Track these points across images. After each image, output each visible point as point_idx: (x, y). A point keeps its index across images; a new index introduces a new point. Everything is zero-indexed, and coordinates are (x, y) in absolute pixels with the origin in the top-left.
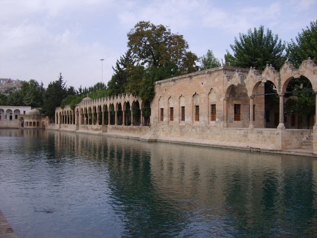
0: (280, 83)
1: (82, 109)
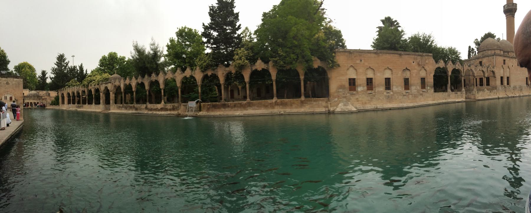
0: (463, 71)
1: (69, 94)
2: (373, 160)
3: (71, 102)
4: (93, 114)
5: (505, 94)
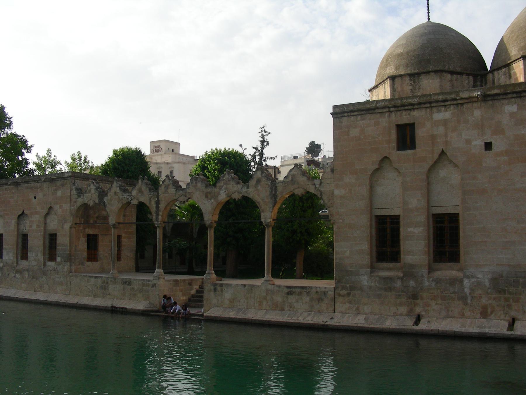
0: (157, 207)
2: (29, 392)
3: (202, 299)
4: (4, 297)
5: (403, 310)
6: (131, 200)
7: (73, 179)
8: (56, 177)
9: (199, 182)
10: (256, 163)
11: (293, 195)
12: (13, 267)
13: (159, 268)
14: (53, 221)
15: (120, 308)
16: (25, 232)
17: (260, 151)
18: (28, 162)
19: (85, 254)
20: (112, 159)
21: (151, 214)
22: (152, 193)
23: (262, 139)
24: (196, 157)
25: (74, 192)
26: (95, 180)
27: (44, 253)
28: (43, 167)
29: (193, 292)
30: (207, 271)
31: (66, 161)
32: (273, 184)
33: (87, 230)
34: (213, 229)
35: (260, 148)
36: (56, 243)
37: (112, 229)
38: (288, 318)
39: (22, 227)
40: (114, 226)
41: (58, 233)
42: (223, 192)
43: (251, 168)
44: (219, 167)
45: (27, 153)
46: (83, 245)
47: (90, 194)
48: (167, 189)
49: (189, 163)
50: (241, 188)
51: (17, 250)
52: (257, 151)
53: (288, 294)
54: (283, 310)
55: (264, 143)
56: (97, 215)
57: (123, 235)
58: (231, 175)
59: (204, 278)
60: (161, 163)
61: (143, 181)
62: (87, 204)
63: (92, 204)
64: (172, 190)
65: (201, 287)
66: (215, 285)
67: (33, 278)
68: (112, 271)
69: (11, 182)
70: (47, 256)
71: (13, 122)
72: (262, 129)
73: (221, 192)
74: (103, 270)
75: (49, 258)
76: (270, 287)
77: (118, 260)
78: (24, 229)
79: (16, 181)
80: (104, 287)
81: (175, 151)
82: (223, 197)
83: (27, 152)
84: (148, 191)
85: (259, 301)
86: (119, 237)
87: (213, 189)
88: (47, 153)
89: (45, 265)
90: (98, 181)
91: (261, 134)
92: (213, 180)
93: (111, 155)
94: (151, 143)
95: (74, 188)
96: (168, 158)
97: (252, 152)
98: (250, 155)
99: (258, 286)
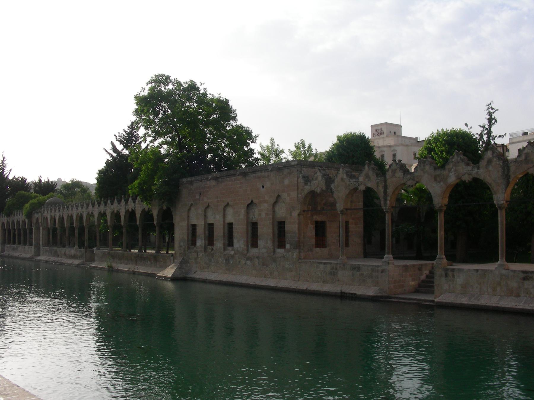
0: (385, 192)
6: (358, 185)
7: (300, 167)
8: (283, 166)
9: (427, 164)
10: (484, 142)
11: (527, 175)
12: (244, 255)
13: (388, 253)
14: (281, 209)
15: (349, 293)
16: (254, 220)
17: (487, 129)
18: (254, 152)
19: (314, 241)
20: (336, 146)
21: (378, 198)
22: (379, 178)
23: (489, 117)
24: (419, 138)
25: (301, 180)
26: (321, 167)
27: (273, 240)
28: (268, 156)
29: (423, 277)
30: (438, 256)
31: (290, 150)
32: (505, 164)
33: (315, 217)
34: (443, 213)
35: (487, 127)
36: (285, 230)
37: (340, 215)
38: (525, 305)
39: (251, 216)
40: (342, 212)
41: (287, 221)
42: (453, 175)
43: (480, 148)
44: (447, 149)
45: (252, 143)
46: (311, 231)
47: (317, 182)
48: (395, 173)
49: (412, 145)
50: (471, 170)
51: (247, 238)
52: (484, 130)
53: (524, 279)
54: (518, 296)
55: (491, 120)
56: (324, 202)
57: (351, 221)
58: (460, 156)
59: (435, 264)
60: (382, 147)
61: (370, 166)
62: (314, 191)
63: (319, 191)
64: (400, 174)
65: (432, 272)
66: (446, 270)
67: (263, 265)
68: (340, 257)
69: (239, 172)
70: (276, 244)
71: (237, 115)
72: (488, 106)
73: (451, 174)
74: (331, 256)
75: (278, 245)
76: (504, 272)
77: (346, 247)
78: (254, 218)
79: (244, 171)
80: (333, 273)
81: (397, 134)
82: (452, 179)
83: (252, 142)
84: (375, 176)
85: (492, 287)
86: (347, 223)
87: (442, 172)
88: (270, 143)
89: (274, 252)
90: (324, 168)
91: (488, 111)
92: (440, 162)
93: (335, 141)
94: (372, 126)
95: (300, 176)
96: (390, 141)
97: (479, 130)
98: (478, 134)
99: (491, 271)
